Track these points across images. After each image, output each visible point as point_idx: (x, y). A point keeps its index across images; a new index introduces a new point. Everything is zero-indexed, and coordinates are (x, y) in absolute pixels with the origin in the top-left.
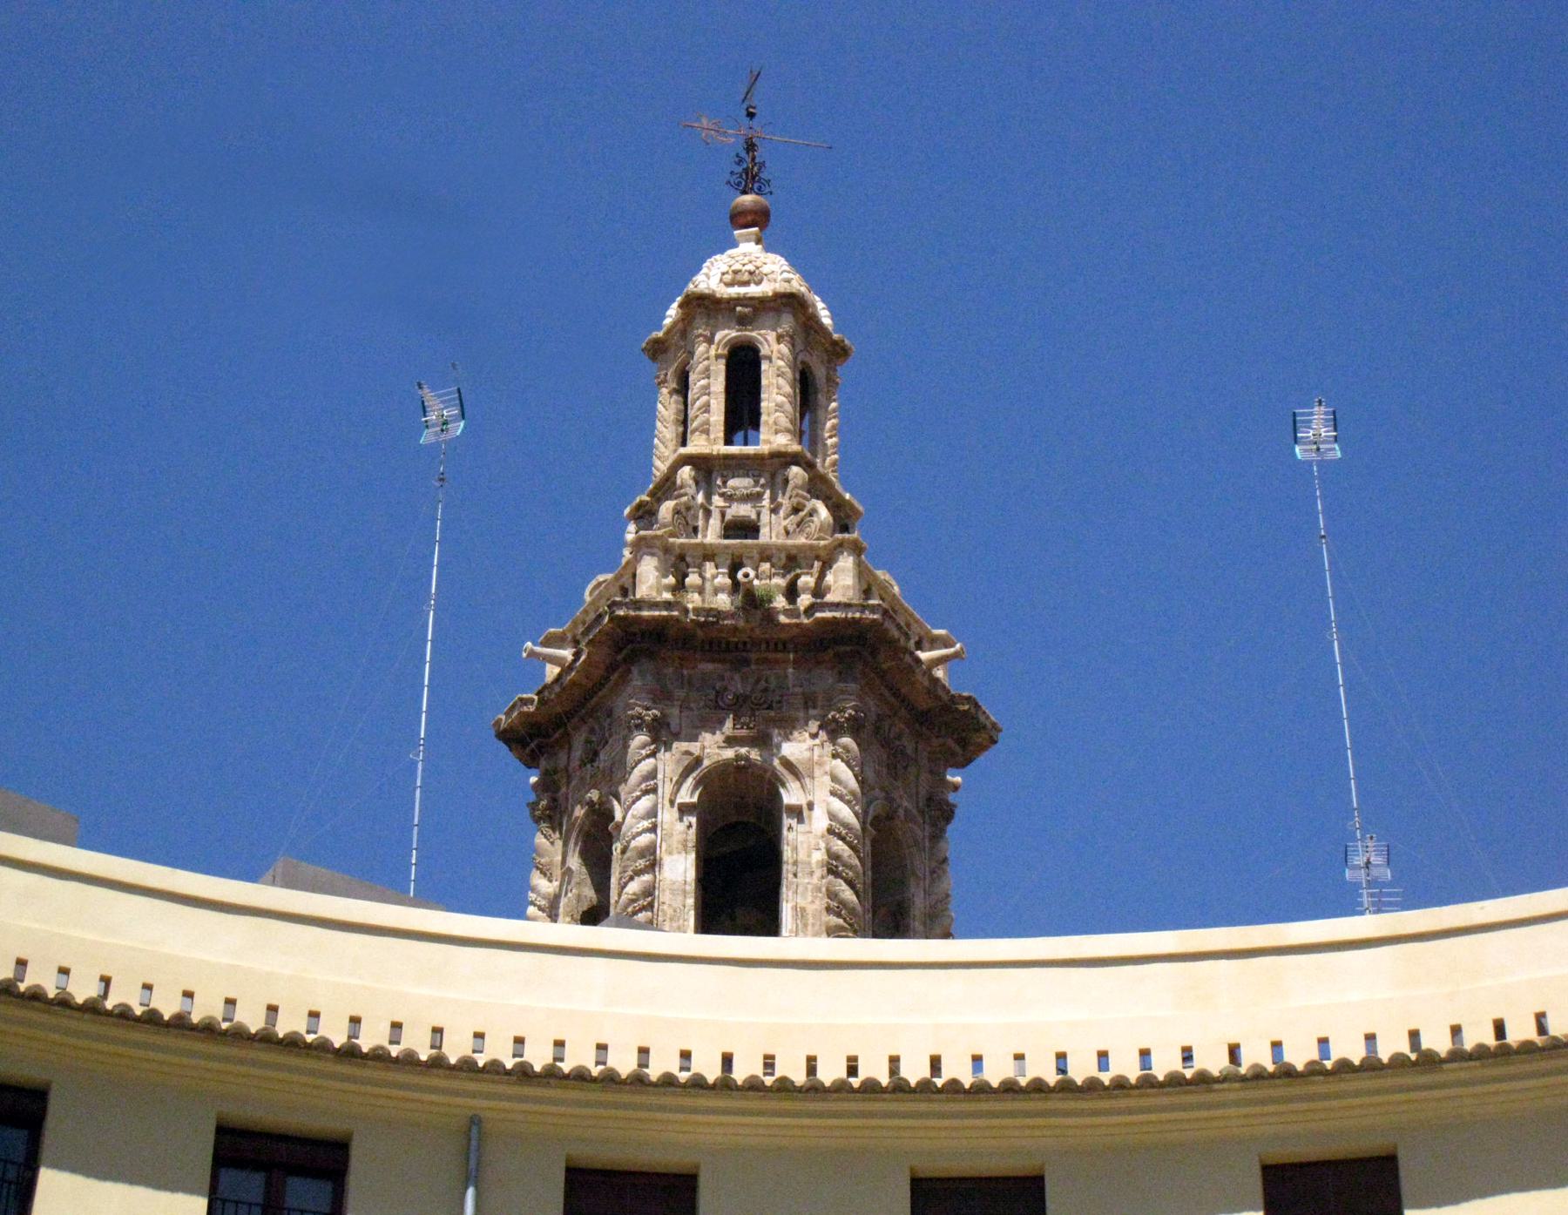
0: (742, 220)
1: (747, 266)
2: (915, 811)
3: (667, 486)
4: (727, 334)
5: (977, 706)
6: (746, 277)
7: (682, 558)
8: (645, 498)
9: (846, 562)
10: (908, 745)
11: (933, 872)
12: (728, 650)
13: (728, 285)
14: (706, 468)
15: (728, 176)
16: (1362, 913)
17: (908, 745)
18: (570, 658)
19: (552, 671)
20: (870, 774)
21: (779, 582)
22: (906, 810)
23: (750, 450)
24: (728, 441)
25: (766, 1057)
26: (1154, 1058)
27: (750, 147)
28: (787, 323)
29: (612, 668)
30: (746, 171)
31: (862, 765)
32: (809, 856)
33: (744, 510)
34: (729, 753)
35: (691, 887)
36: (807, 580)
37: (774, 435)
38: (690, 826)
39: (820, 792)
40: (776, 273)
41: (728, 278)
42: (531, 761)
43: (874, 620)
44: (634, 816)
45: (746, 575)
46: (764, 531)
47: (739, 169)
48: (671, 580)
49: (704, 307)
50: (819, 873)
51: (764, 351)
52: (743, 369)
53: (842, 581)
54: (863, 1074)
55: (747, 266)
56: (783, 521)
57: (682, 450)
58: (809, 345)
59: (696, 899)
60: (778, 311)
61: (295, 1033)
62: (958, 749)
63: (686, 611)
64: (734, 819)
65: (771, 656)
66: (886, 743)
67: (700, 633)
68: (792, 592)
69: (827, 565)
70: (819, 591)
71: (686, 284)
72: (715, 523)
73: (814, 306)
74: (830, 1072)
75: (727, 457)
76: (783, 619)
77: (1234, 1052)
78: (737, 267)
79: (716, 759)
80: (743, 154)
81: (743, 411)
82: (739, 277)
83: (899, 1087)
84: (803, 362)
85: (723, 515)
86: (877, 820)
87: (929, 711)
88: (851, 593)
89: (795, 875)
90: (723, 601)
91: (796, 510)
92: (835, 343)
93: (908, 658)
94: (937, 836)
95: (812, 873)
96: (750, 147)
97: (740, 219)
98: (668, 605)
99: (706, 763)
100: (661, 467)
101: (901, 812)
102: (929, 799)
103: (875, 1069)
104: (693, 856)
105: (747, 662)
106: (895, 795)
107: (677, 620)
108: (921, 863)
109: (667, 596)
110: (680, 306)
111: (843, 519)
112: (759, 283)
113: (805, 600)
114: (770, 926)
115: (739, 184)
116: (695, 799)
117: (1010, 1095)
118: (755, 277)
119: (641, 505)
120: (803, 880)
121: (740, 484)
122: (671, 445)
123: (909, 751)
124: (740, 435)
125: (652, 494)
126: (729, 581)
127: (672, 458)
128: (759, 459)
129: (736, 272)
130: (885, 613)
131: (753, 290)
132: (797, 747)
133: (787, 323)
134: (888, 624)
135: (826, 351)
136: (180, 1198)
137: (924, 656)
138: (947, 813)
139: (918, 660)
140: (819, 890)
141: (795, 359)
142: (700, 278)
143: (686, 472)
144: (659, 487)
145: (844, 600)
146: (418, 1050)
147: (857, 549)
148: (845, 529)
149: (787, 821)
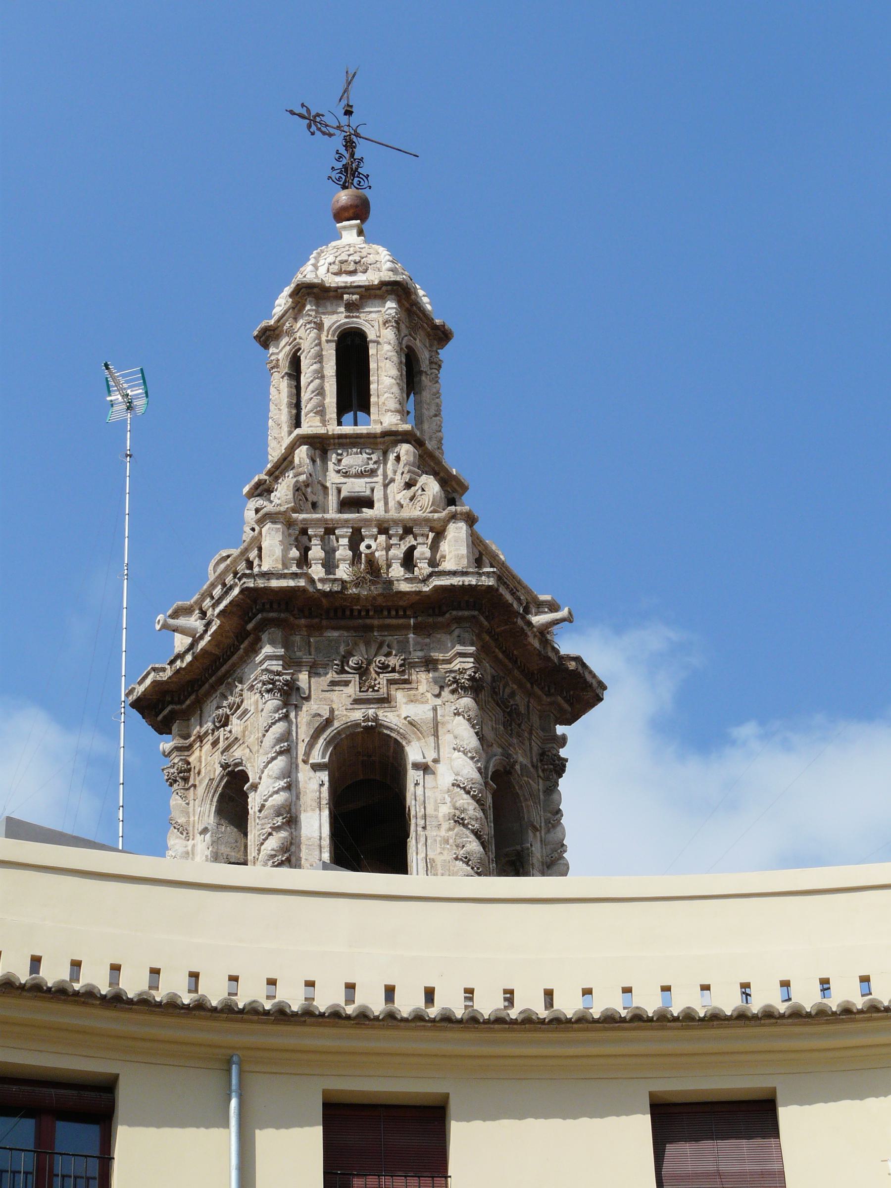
0: (346, 215)
1: (348, 255)
2: (530, 766)
3: (285, 463)
4: (336, 319)
5: (584, 665)
6: (352, 267)
7: (304, 532)
8: (263, 477)
9: (457, 532)
10: (520, 700)
11: (548, 822)
12: (352, 616)
13: (339, 273)
14: (321, 445)
15: (329, 172)
16: (526, 874)
17: (520, 700)
18: (201, 629)
19: (181, 642)
20: (490, 735)
21: (398, 552)
22: (521, 765)
23: (361, 429)
24: (340, 424)
25: (506, 992)
26: (753, 991)
27: (349, 144)
28: (390, 307)
29: (242, 635)
30: (345, 167)
31: (481, 724)
32: (436, 810)
33: (357, 487)
34: (357, 715)
35: (326, 842)
36: (422, 551)
37: (385, 410)
38: (322, 785)
39: (443, 751)
40: (381, 265)
41: (335, 268)
42: (163, 728)
43: (489, 587)
44: (269, 776)
45: (369, 547)
46: (379, 505)
47: (339, 165)
48: (294, 553)
49: (312, 294)
50: (445, 826)
51: (371, 335)
52: (352, 350)
53: (455, 550)
55: (348, 255)
56: (397, 493)
57: (298, 431)
58: (413, 329)
59: (330, 853)
60: (383, 298)
61: (63, 981)
62: (566, 706)
63: (312, 581)
64: (361, 777)
65: (394, 621)
66: (502, 704)
67: (324, 601)
68: (408, 561)
69: (440, 535)
71: (294, 274)
72: (332, 501)
73: (416, 294)
75: (341, 436)
76: (404, 587)
78: (344, 257)
79: (345, 720)
80: (343, 150)
81: (354, 392)
82: (344, 267)
84: (408, 347)
85: (339, 491)
86: (496, 776)
87: (298, 689)
88: (465, 562)
89: (424, 828)
90: (343, 572)
91: (409, 485)
92: (436, 327)
93: (520, 622)
94: (552, 789)
95: (439, 826)
96: (349, 144)
97: (341, 215)
98: (295, 576)
99: (336, 724)
100: (275, 452)
101: (518, 767)
102: (543, 754)
104: (326, 813)
105: (370, 628)
106: (511, 751)
107: (303, 590)
108: (536, 815)
109: (294, 569)
110: (291, 295)
111: (453, 490)
112: (365, 271)
113: (422, 568)
114: (396, 862)
115: (339, 179)
116: (326, 760)
117: (742, 1023)
119: (259, 484)
120: (431, 833)
121: (353, 460)
122: (285, 428)
123: (522, 710)
124: (349, 417)
125: (270, 473)
126: (350, 553)
127: (287, 441)
128: (369, 436)
129: (342, 262)
130: (499, 579)
131: (360, 279)
133: (390, 307)
134: (502, 590)
135: (429, 335)
136: (296, 1132)
137: (538, 620)
138: (560, 767)
139: (529, 624)
140: (447, 841)
141: (400, 343)
142: (308, 268)
143: (302, 453)
144: (277, 466)
145: (460, 569)
146: (209, 997)
147: (470, 520)
148: (451, 502)
149: (413, 775)
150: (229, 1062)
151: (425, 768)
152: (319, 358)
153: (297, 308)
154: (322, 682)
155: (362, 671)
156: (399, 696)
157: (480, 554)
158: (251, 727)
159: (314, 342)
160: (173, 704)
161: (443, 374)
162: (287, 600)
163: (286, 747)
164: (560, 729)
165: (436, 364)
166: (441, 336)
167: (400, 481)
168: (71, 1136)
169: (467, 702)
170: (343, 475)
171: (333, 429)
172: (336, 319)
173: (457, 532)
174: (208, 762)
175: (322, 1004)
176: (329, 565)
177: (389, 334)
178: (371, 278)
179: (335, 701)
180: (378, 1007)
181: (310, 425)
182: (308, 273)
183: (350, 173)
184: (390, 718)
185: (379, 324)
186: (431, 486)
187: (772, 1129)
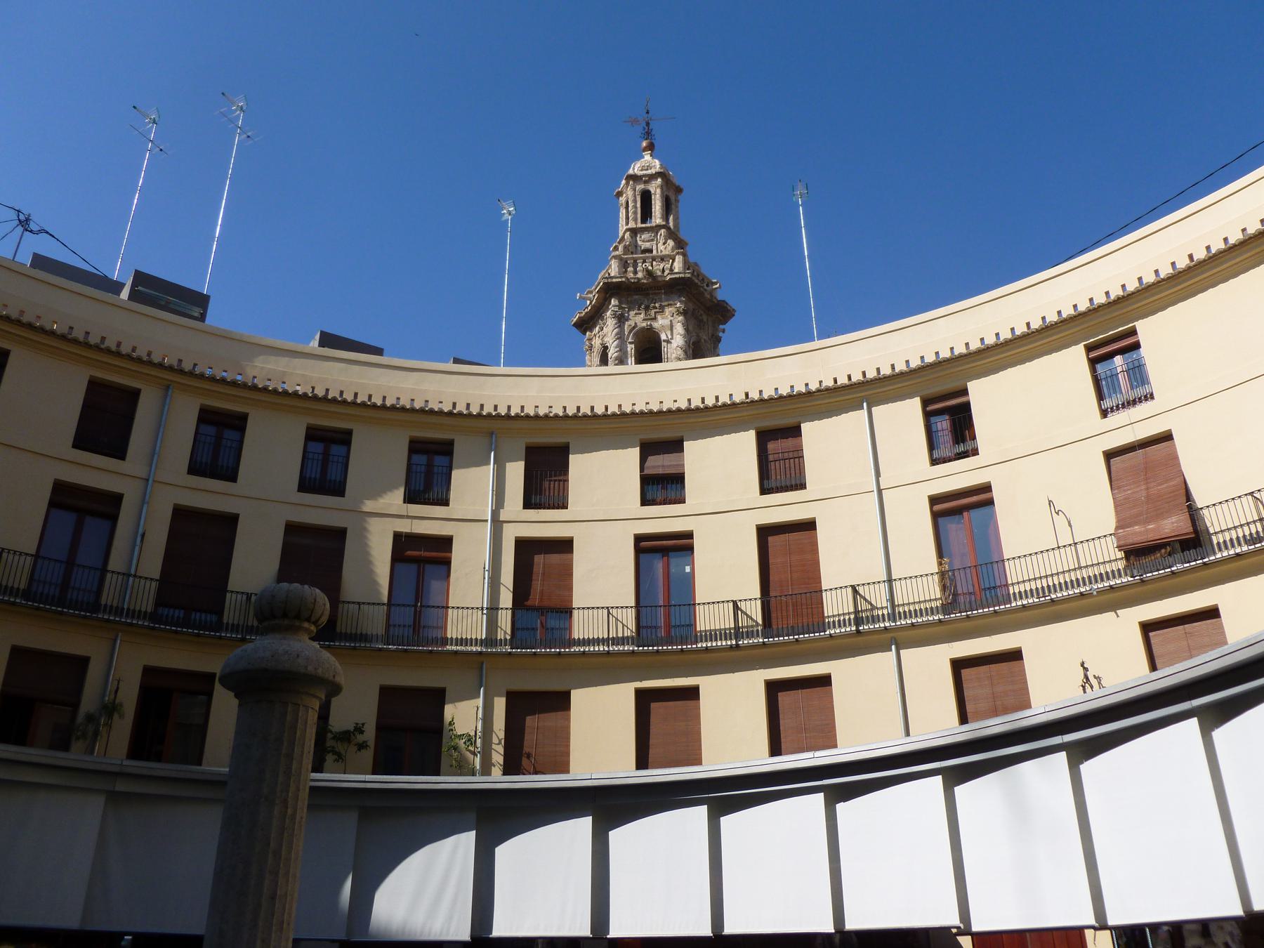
3: (623, 239)
4: (640, 187)
10: (705, 318)
14: (634, 232)
17: (705, 318)
20: (691, 328)
27: (648, 124)
33: (648, 245)
34: (644, 324)
37: (657, 219)
40: (656, 165)
49: (635, 178)
52: (646, 197)
53: (678, 265)
54: (582, 411)
55: (648, 163)
56: (661, 247)
58: (668, 189)
70: (671, 270)
74: (571, 412)
77: (893, 367)
83: (595, 416)
90: (640, 275)
96: (648, 124)
100: (621, 234)
103: (585, 410)
105: (648, 294)
113: (667, 272)
118: (649, 168)
121: (645, 236)
131: (649, 172)
132: (661, 322)
143: (628, 234)
150: (492, 433)
151: (668, 342)
152: (635, 201)
153: (627, 184)
154: (632, 313)
155: (647, 308)
156: (659, 317)
157: (687, 265)
158: (607, 332)
159: (630, 194)
160: (587, 324)
161: (680, 204)
162: (619, 285)
163: (620, 337)
164: (721, 327)
165: (677, 201)
166: (679, 190)
167: (661, 242)
168: (230, 434)
169: (681, 318)
170: (643, 241)
171: (640, 225)
172: (640, 187)
173: (679, 259)
174: (597, 343)
175: (541, 413)
176: (635, 272)
177: (658, 191)
178: (653, 171)
179: (637, 319)
180: (114, 348)
181: (632, 225)
182: (631, 172)
183: (648, 134)
184: (656, 325)
185: (655, 188)
186: (671, 243)
187: (681, 450)
